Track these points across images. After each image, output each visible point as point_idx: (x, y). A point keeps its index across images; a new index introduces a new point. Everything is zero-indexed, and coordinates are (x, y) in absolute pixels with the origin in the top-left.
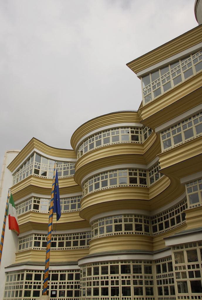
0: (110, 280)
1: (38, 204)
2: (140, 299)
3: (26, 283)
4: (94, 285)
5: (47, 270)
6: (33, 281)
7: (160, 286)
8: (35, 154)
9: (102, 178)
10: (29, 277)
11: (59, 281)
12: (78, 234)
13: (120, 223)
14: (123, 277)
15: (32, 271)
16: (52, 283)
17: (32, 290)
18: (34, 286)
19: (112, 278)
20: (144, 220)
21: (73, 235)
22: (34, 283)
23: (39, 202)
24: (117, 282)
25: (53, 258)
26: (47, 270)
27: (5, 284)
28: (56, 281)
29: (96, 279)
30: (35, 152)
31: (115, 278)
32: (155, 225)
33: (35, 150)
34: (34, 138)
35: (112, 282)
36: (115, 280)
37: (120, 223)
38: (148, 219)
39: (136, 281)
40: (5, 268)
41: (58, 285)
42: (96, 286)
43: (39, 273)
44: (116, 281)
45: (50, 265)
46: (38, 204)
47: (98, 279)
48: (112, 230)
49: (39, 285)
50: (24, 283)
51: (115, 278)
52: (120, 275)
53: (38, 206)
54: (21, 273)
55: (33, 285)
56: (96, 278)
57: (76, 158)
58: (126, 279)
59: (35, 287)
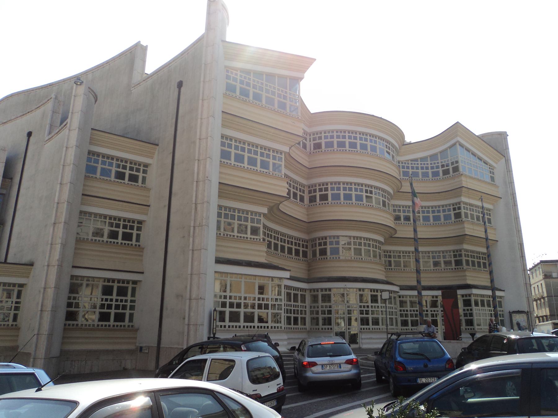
1: (471, 318)
6: (114, 297)
13: (332, 140)
14: (431, 311)
17: (113, 311)
20: (373, 245)
25: (262, 251)
27: (66, 298)
32: (314, 248)
34: (212, 359)
37: (332, 140)
38: (370, 241)
39: (363, 310)
44: (107, 304)
46: (471, 318)
47: (318, 307)
55: (114, 303)
56: (375, 306)
59: (117, 307)
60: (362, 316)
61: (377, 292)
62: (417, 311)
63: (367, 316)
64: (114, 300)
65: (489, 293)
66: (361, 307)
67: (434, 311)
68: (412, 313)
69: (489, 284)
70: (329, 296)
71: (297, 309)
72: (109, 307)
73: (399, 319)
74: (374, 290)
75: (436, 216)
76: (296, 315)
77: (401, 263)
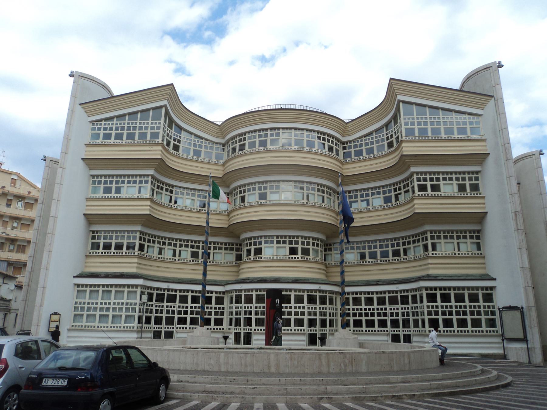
0: (154, 308)
2: (405, 342)
3: (428, 307)
4: (147, 312)
5: (203, 291)
7: (231, 317)
8: (401, 104)
9: (106, 182)
10: (381, 301)
11: (177, 304)
12: (409, 238)
15: (188, 291)
16: (167, 307)
18: (377, 313)
19: (391, 309)
21: (403, 239)
22: (191, 307)
23: (477, 179)
24: (397, 314)
26: (203, 291)
28: (250, 305)
29: (149, 306)
30: (400, 101)
31: (248, 307)
33: (399, 97)
35: (157, 310)
36: (159, 308)
39: (404, 312)
40: (74, 277)
41: (253, 310)
42: (149, 314)
43: (186, 294)
45: (346, 286)
47: (152, 306)
48: (19, 252)
49: (359, 311)
50: (425, 307)
51: (394, 309)
52: (318, 305)
53: (478, 185)
54: (418, 293)
55: (189, 310)
57: (224, 138)
58: (394, 311)
60: (404, 318)
61: (316, 292)
62: (135, 304)
63: (408, 318)
64: (213, 308)
65: (199, 288)
66: (76, 303)
67: (312, 308)
68: (380, 311)
69: (201, 277)
70: (491, 295)
71: (416, 310)
72: (186, 313)
73: (426, 318)
74: (431, 289)
75: (422, 128)
76: (416, 317)
77: (377, 254)
